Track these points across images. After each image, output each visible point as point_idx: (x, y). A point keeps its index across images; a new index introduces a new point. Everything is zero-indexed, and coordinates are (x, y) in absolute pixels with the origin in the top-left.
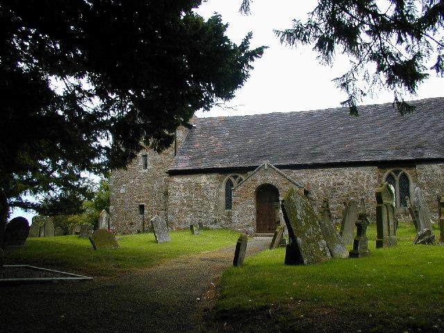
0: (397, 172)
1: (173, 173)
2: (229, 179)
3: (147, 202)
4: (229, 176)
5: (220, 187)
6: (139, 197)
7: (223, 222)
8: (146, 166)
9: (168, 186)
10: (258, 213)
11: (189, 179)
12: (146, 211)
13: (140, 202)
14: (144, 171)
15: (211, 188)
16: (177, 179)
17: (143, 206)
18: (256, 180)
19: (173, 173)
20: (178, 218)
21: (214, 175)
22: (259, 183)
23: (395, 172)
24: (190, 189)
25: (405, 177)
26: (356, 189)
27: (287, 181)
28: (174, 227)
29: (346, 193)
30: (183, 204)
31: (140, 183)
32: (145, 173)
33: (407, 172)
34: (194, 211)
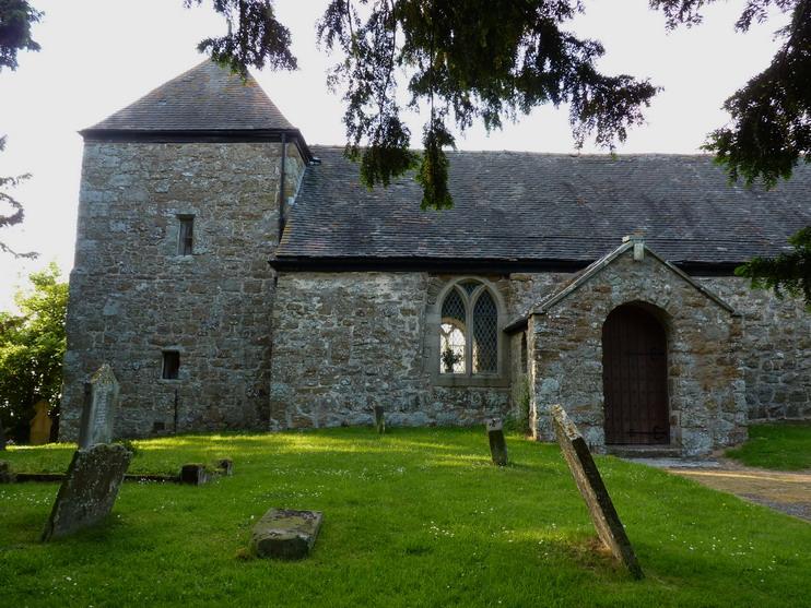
0: (470, 286)
1: (286, 265)
2: (454, 291)
3: (185, 343)
4: (454, 282)
5: (428, 309)
6: (163, 330)
7: (438, 405)
8: (188, 243)
9: (273, 300)
10: (609, 378)
11: (338, 284)
12: (184, 370)
13: (164, 345)
14: (181, 258)
15: (405, 312)
16: (303, 283)
17: (176, 354)
18: (608, 290)
19: (286, 265)
20: (303, 391)
21: (415, 278)
22: (618, 296)
23: (464, 285)
24: (343, 311)
25: (486, 300)
26: (790, 332)
27: (697, 298)
28: (288, 417)
29: (764, 340)
30: (319, 351)
31: (169, 290)
32: (185, 264)
33: (493, 287)
34: (355, 372)
